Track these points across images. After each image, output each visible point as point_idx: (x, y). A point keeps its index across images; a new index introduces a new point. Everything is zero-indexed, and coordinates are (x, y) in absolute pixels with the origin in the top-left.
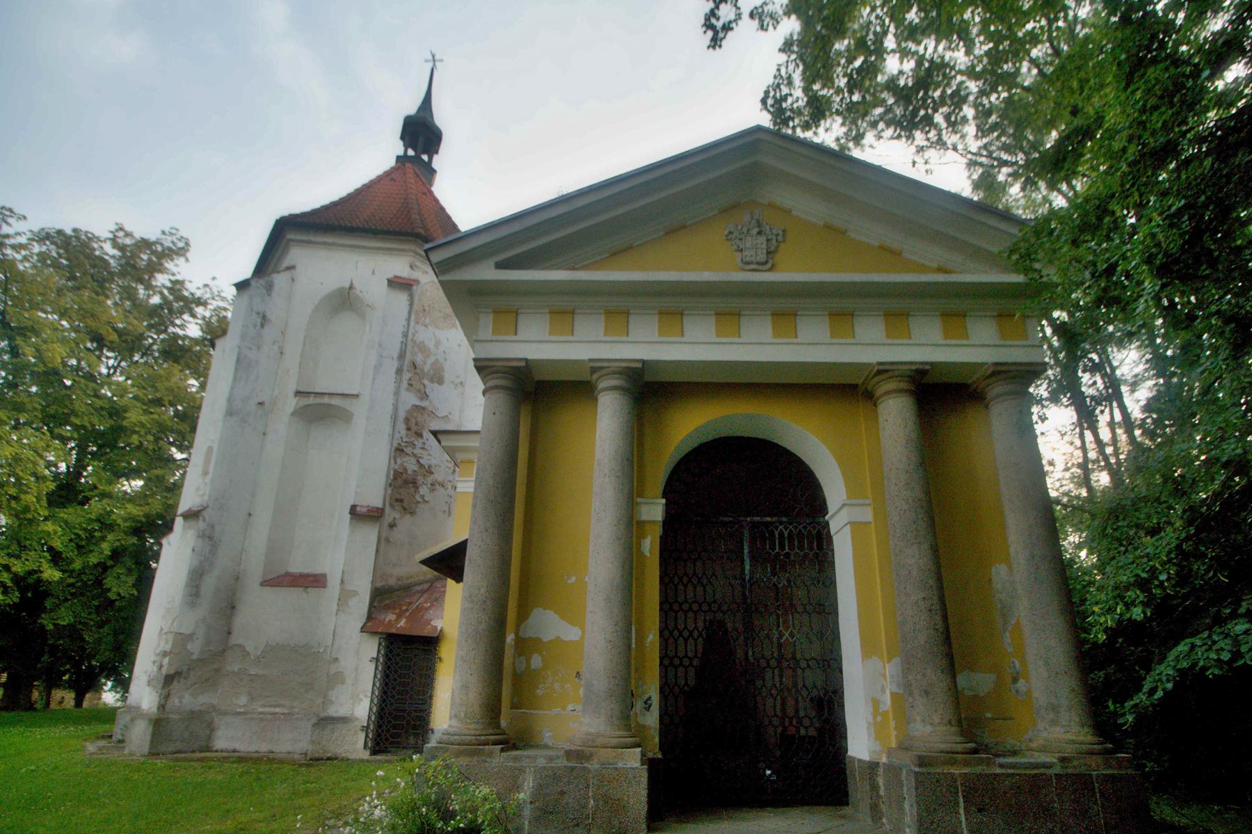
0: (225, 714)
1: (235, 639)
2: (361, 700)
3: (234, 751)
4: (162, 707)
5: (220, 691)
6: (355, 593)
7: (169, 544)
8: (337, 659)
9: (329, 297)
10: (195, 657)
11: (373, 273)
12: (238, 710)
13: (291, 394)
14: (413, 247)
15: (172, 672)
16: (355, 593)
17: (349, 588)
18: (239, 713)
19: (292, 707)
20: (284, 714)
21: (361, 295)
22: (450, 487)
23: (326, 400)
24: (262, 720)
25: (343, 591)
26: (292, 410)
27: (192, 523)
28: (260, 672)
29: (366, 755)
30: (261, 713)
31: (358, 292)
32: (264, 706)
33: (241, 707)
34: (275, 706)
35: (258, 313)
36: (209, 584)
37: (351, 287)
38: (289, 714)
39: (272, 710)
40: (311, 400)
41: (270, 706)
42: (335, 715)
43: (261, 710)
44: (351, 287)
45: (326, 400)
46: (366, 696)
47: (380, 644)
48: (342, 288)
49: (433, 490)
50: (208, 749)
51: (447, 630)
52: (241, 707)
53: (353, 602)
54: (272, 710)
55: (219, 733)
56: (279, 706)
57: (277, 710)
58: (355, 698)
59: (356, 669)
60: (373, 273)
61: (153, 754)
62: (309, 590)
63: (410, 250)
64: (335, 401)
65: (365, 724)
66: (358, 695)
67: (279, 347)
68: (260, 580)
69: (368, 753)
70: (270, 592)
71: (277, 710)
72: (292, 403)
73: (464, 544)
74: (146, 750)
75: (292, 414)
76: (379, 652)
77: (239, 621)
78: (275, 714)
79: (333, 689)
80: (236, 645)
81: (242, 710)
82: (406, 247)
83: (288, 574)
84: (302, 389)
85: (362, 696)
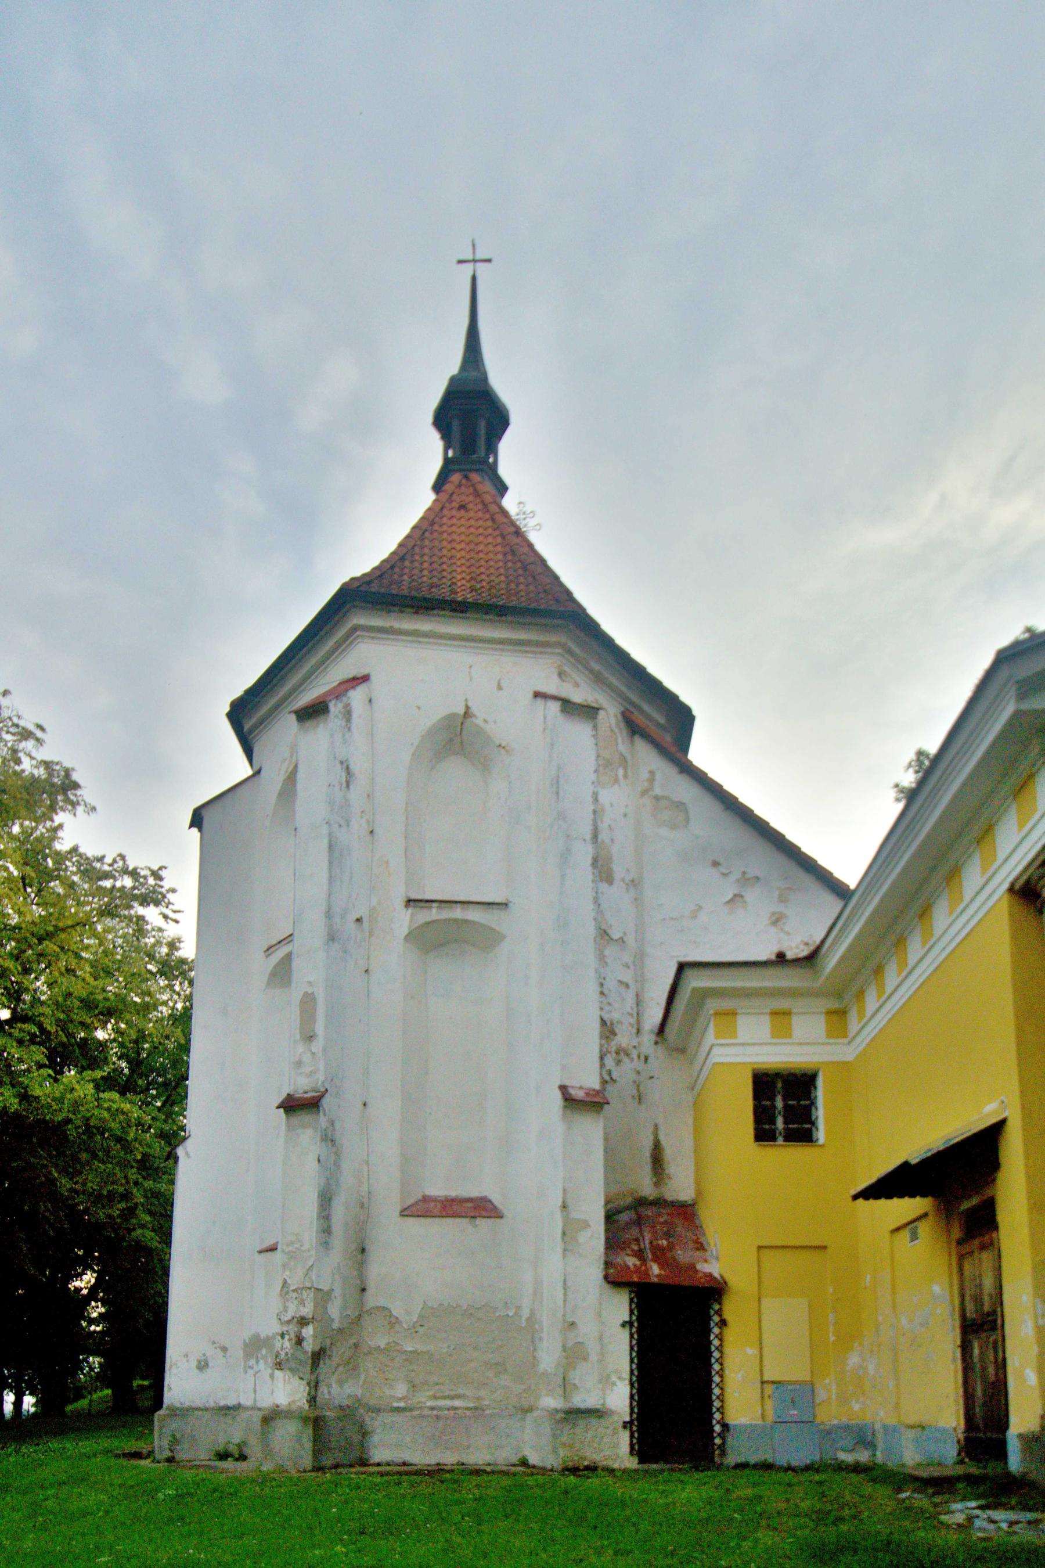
0: (379, 1410)
1: (372, 1300)
2: (614, 1384)
3: (404, 1464)
4: (312, 1400)
5: (363, 1376)
6: (585, 1224)
7: (187, 1154)
8: (573, 1324)
9: (432, 733)
10: (336, 1325)
11: (500, 688)
12: (395, 1404)
13: (399, 903)
14: (563, 639)
15: (317, 1349)
16: (585, 1224)
17: (575, 1215)
18: (398, 1410)
19: (478, 1398)
20: (467, 1409)
21: (488, 728)
22: (635, 1056)
23: (458, 913)
24: (437, 1417)
25: (567, 1221)
26: (406, 931)
27: (305, 1117)
28: (421, 1347)
29: (632, 1463)
30: (432, 1408)
31: (479, 722)
32: (435, 1398)
33: (400, 1399)
34: (452, 1398)
35: (342, 763)
36: (339, 1212)
37: (467, 714)
38: (476, 1408)
39: (449, 1403)
40: (434, 914)
41: (444, 1398)
42: (582, 1406)
43: (429, 1404)
44: (467, 714)
45: (458, 913)
46: (620, 1378)
47: (631, 1300)
48: (453, 716)
49: (619, 1062)
50: (363, 1462)
51: (731, 1279)
52: (400, 1399)
53: (583, 1237)
54: (449, 1403)
55: (375, 1439)
56: (458, 1397)
57: (457, 1403)
58: (606, 1381)
59: (601, 1338)
60: (500, 688)
61: (318, 1469)
62: (478, 1221)
63: (558, 644)
64: (474, 915)
65: (628, 1419)
66: (608, 1377)
67: (368, 821)
68: (399, 1209)
69: (635, 1460)
70: (414, 1225)
71: (457, 1403)
72: (403, 920)
73: (993, 1135)
74: (307, 1462)
75: (407, 938)
76: (631, 1312)
77: (375, 1271)
78: (455, 1408)
79: (575, 1369)
80: (378, 1308)
81: (402, 1404)
82: (553, 638)
83: (426, 1199)
84: (414, 896)
85: (614, 1378)
